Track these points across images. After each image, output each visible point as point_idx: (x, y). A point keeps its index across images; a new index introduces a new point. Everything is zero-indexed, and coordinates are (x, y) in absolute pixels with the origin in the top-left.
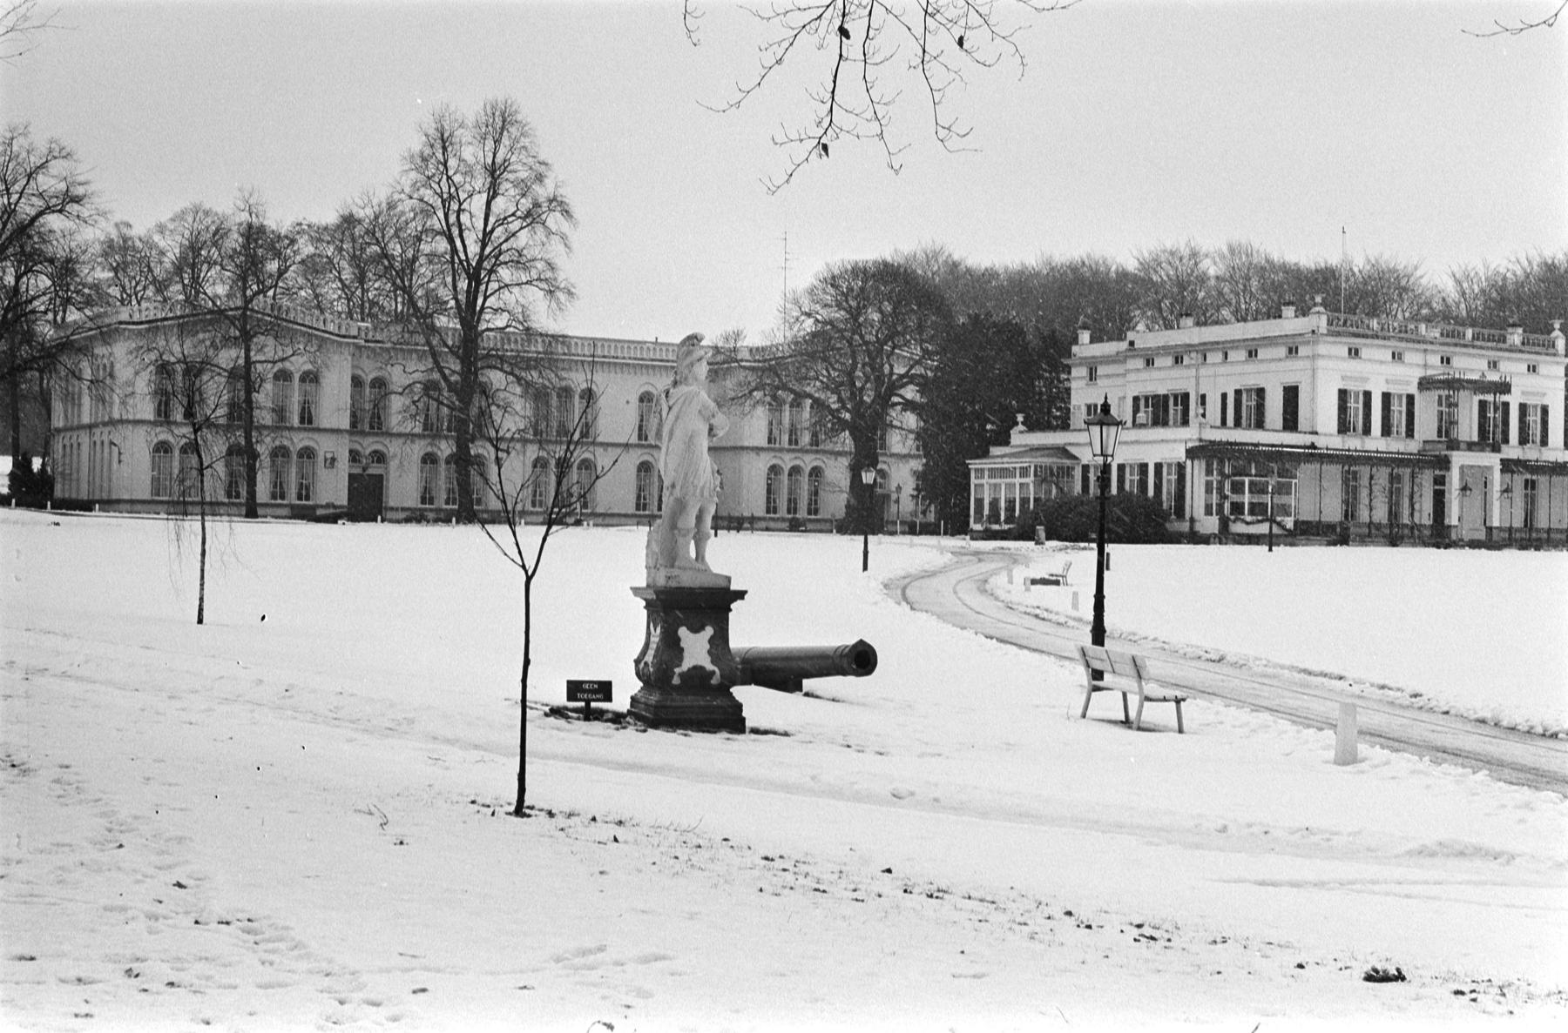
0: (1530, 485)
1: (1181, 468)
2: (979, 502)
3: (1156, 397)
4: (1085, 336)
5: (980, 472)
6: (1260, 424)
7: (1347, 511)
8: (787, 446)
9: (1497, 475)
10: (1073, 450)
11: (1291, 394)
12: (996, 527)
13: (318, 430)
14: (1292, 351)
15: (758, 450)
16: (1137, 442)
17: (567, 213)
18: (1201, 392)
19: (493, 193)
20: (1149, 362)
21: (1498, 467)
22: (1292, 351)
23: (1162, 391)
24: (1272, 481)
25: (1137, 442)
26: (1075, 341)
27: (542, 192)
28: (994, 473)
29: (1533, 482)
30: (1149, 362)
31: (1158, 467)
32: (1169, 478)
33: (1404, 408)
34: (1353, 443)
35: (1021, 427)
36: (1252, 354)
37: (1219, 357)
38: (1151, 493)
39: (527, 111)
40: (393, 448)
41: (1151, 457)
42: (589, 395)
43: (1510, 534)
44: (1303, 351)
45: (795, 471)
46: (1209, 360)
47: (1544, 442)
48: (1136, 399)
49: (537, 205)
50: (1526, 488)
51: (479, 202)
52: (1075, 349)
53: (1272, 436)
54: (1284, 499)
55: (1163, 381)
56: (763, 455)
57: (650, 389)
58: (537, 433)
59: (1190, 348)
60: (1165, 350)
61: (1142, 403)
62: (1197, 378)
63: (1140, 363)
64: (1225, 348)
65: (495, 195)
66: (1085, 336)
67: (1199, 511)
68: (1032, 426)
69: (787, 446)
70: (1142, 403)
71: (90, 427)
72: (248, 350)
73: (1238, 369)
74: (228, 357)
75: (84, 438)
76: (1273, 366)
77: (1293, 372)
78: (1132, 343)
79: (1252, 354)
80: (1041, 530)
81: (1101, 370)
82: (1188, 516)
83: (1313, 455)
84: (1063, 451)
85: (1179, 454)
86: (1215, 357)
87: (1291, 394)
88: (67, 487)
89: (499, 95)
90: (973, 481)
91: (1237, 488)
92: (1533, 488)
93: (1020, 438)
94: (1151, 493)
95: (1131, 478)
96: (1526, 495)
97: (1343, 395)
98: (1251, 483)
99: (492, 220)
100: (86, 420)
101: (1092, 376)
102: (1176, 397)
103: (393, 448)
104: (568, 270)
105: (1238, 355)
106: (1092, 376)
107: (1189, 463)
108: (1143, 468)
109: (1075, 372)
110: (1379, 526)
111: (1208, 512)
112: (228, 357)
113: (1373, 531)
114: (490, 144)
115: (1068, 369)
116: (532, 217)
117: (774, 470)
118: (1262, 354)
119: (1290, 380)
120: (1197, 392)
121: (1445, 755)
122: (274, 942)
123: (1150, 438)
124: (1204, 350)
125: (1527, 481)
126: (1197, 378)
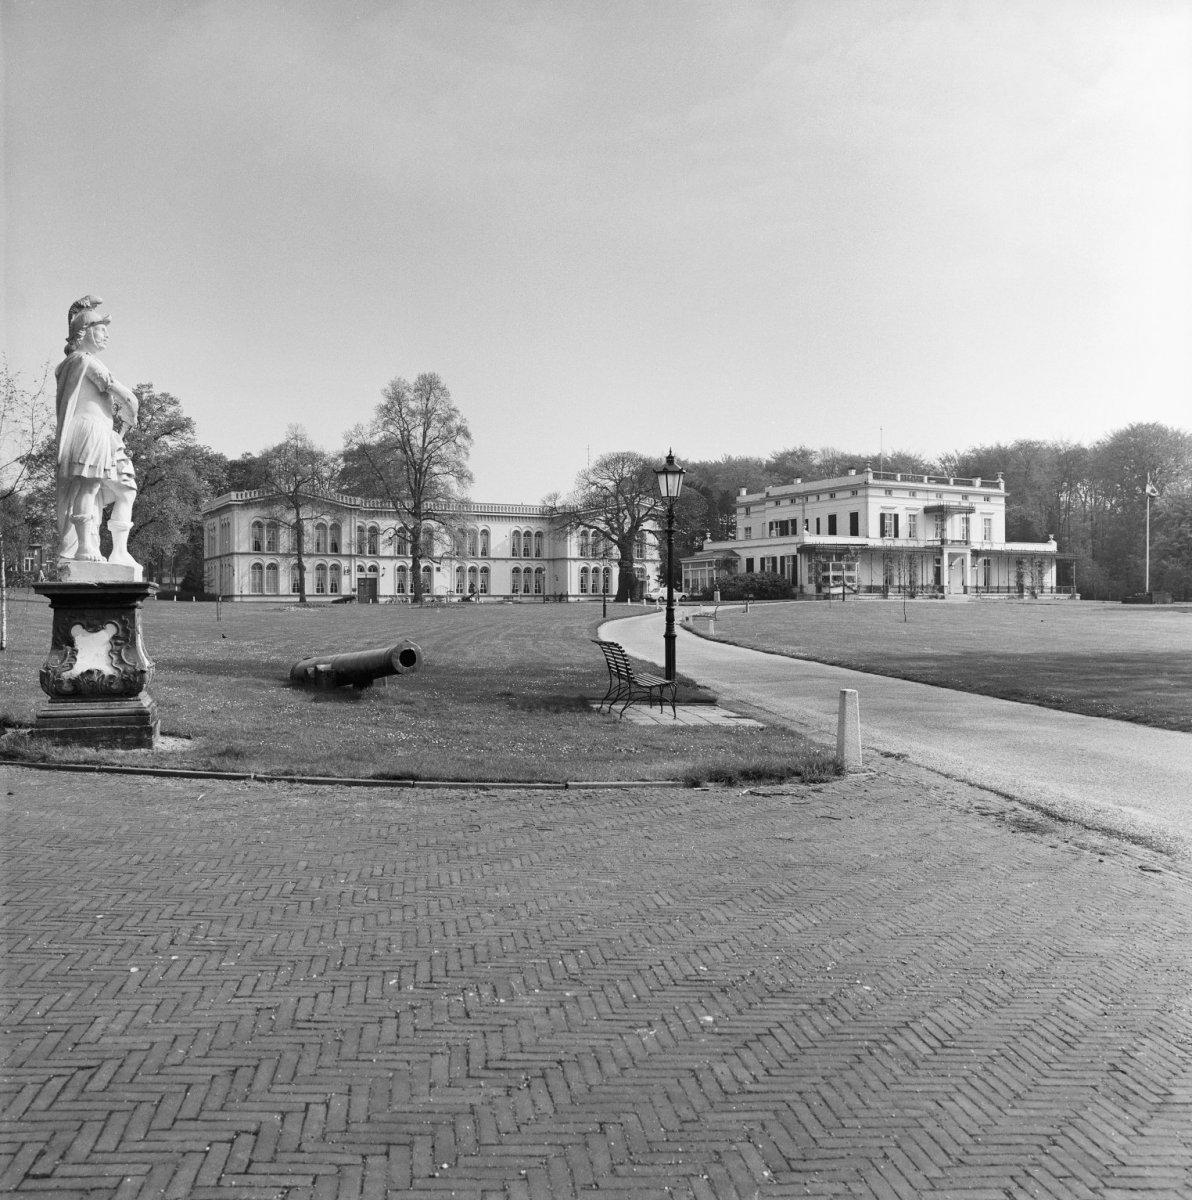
0: (987, 563)
1: (795, 557)
2: (687, 581)
3: (781, 522)
4: (744, 492)
5: (687, 565)
6: (833, 531)
8: (480, 556)
9: (969, 558)
10: (737, 551)
11: (854, 517)
12: (696, 594)
13: (490, 559)
14: (854, 493)
15: (575, 560)
16: (770, 546)
17: (467, 436)
19: (427, 425)
20: (777, 503)
21: (969, 553)
22: (854, 493)
23: (785, 518)
24: (844, 564)
25: (770, 546)
26: (739, 494)
27: (456, 422)
28: (694, 565)
29: (989, 561)
30: (777, 503)
31: (782, 558)
32: (788, 563)
33: (893, 522)
34: (888, 542)
35: (709, 540)
37: (814, 498)
38: (779, 572)
39: (445, 381)
40: (382, 564)
41: (778, 553)
42: (486, 533)
44: (860, 493)
45: (596, 570)
46: (821, 499)
47: (896, 535)
48: (771, 524)
49: (450, 432)
51: (420, 430)
52: (738, 499)
53: (843, 539)
54: (851, 574)
55: (785, 513)
56: (510, 562)
57: (529, 530)
58: (458, 553)
59: (799, 495)
60: (784, 497)
61: (774, 526)
62: (804, 511)
63: (773, 504)
64: (818, 494)
65: (429, 427)
66: (744, 492)
67: (805, 582)
68: (715, 539)
69: (329, 553)
70: (774, 526)
71: (220, 557)
72: (298, 514)
73: (825, 504)
74: (291, 517)
75: (217, 563)
76: (843, 502)
77: (853, 505)
78: (768, 493)
79: (832, 496)
80: (718, 594)
81: (752, 509)
82: (799, 584)
83: (866, 552)
84: (731, 552)
85: (793, 551)
86: (812, 499)
87: (854, 517)
89: (427, 372)
90: (683, 570)
91: (826, 568)
93: (709, 545)
94: (779, 572)
95: (768, 565)
97: (883, 516)
98: (833, 565)
99: (427, 440)
100: (218, 554)
101: (748, 512)
102: (777, 523)
103: (382, 564)
104: (470, 465)
105: (826, 497)
106: (748, 512)
107: (799, 555)
109: (738, 511)
111: (810, 582)
112: (291, 517)
114: (424, 401)
115: (735, 512)
116: (447, 439)
117: (584, 570)
118: (838, 495)
119: (853, 509)
121: (477, 772)
124: (805, 495)
126: (804, 511)
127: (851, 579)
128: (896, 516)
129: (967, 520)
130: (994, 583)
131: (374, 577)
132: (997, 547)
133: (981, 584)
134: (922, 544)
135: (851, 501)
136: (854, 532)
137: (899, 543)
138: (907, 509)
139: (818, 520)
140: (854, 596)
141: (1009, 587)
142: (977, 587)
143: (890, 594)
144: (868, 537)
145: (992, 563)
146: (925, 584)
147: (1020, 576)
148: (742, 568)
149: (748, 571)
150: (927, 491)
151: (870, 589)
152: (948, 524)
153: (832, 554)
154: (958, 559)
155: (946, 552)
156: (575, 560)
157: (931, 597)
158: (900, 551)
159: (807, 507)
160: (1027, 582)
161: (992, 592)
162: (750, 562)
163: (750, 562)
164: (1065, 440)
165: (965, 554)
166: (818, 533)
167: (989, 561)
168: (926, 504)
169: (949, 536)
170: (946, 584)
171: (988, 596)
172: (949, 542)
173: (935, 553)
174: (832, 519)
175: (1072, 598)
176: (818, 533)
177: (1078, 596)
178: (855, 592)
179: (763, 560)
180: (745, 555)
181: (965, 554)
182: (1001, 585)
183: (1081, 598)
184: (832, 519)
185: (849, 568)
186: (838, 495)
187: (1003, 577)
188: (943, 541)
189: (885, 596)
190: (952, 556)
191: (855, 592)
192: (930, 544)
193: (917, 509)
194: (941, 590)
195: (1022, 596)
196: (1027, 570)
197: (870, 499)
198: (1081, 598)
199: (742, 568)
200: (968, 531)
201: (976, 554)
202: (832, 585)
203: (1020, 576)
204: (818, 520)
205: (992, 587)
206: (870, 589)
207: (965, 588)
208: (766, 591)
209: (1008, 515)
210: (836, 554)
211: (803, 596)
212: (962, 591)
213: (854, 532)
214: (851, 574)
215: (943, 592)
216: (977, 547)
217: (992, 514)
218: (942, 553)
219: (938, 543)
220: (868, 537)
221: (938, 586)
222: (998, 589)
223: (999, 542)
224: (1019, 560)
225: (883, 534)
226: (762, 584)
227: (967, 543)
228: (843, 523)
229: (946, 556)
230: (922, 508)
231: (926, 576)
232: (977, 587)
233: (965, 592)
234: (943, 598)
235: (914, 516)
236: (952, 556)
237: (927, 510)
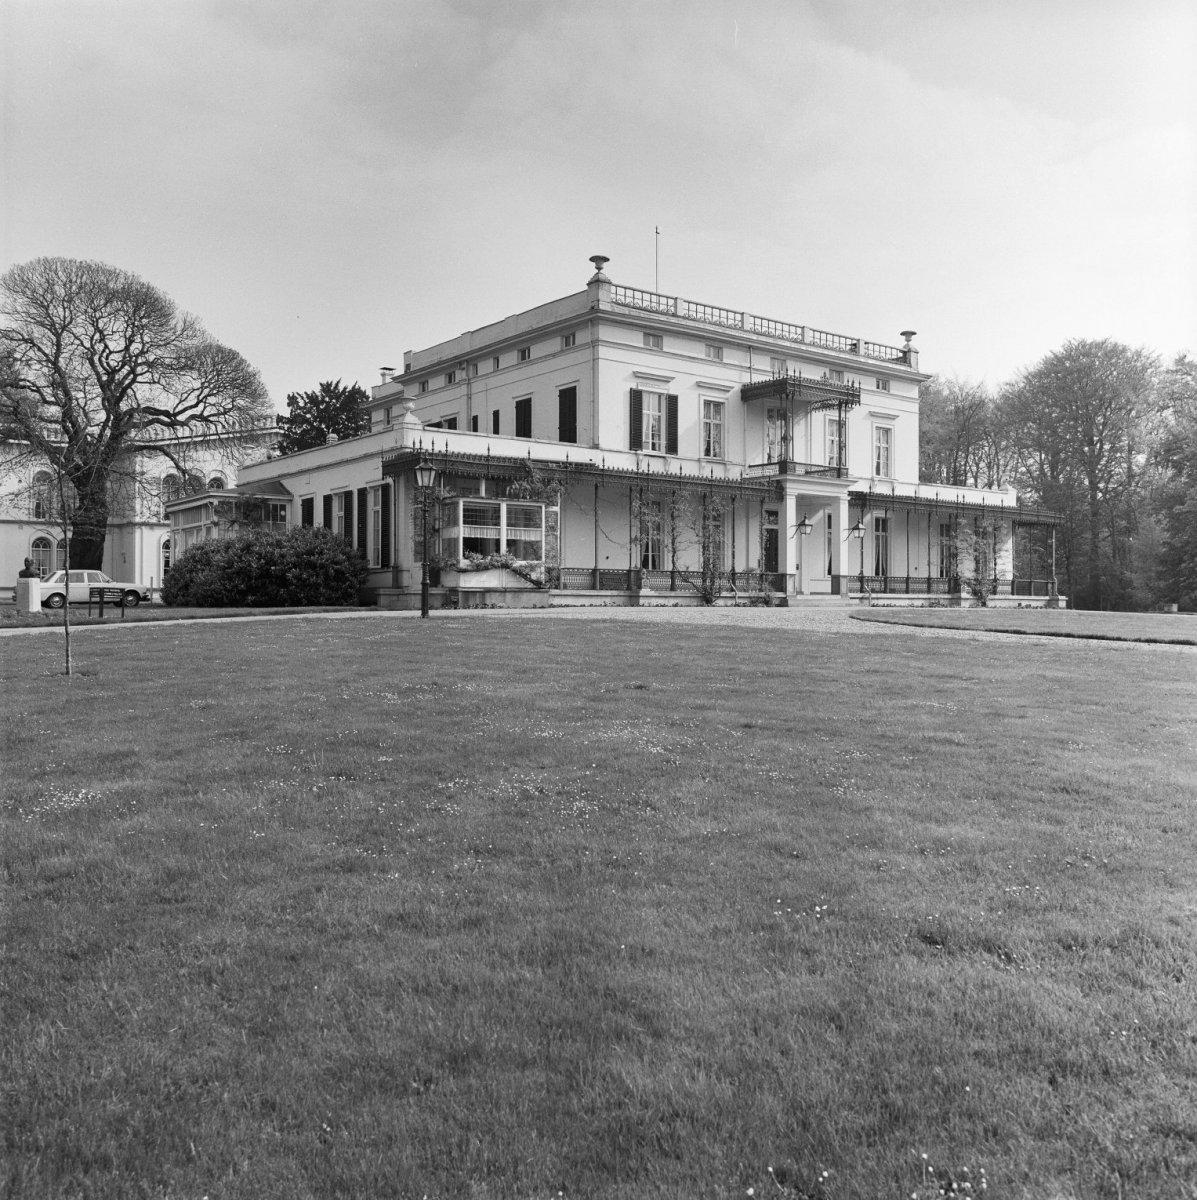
0: (881, 525)
1: (385, 488)
6: (524, 430)
7: (646, 557)
9: (844, 508)
11: (568, 398)
18: (474, 414)
31: (362, 493)
36: (524, 355)
43: (907, 587)
47: (672, 447)
50: (877, 530)
53: (546, 449)
54: (525, 535)
79: (524, 355)
85: (369, 475)
87: (568, 398)
88: (742, 601)
92: (885, 530)
96: (877, 537)
97: (636, 398)
108: (348, 495)
110: (686, 576)
113: (678, 582)
120: (469, 414)
122: (512, 702)
123: (348, 456)
125: (877, 520)
127: (532, 550)
128: (672, 401)
129: (841, 425)
130: (898, 570)
131: (784, 596)
132: (903, 491)
133: (869, 572)
134: (734, 474)
135: (561, 361)
136: (568, 433)
137: (674, 467)
138: (699, 385)
139: (496, 414)
140: (536, 598)
141: (929, 580)
142: (861, 579)
143: (644, 592)
144: (596, 446)
145: (891, 525)
146: (739, 569)
147: (950, 556)
148: (294, 516)
149: (325, 525)
150: (750, 347)
151: (599, 580)
152: (799, 430)
153: (477, 478)
154: (820, 514)
155: (793, 491)
156: (151, 526)
157: (754, 602)
158: (676, 484)
159: (477, 386)
160: (966, 569)
161: (893, 591)
162: (308, 505)
163: (308, 505)
164: (961, 382)
165: (837, 499)
166: (496, 431)
167: (885, 521)
168: (746, 379)
169: (799, 454)
170: (791, 569)
171: (885, 599)
172: (800, 470)
173: (765, 495)
174: (524, 409)
175: (1051, 604)
176: (496, 431)
177: (1063, 600)
178: (538, 586)
179: (328, 500)
180: (299, 489)
181: (837, 499)
182: (913, 574)
183: (1069, 606)
184: (524, 409)
185: (528, 519)
186: (537, 351)
187: (914, 558)
188: (784, 465)
189: (633, 600)
190: (806, 505)
191: (538, 586)
192: (757, 473)
193: (726, 390)
194: (780, 583)
195: (956, 601)
196: (965, 543)
197: (603, 351)
198: (1069, 606)
199: (294, 516)
200: (842, 447)
201: (860, 501)
202: (464, 563)
203: (950, 556)
204: (496, 414)
205: (895, 580)
206: (599, 580)
207: (836, 581)
208: (282, 581)
209: (923, 435)
210: (490, 479)
211: (398, 596)
212: (827, 586)
213: (568, 432)
214: (525, 535)
215: (783, 589)
216: (862, 487)
217: (893, 418)
218: (780, 495)
219: (773, 471)
220: (596, 446)
221: (772, 579)
222: (908, 585)
223: (905, 480)
224: (945, 522)
225: (636, 442)
226: (270, 561)
227: (839, 472)
228: (547, 414)
229: (791, 504)
230: (737, 387)
231: (746, 554)
232: (861, 579)
233: (836, 590)
234: (783, 603)
235: (718, 405)
236: (806, 505)
237: (749, 394)
